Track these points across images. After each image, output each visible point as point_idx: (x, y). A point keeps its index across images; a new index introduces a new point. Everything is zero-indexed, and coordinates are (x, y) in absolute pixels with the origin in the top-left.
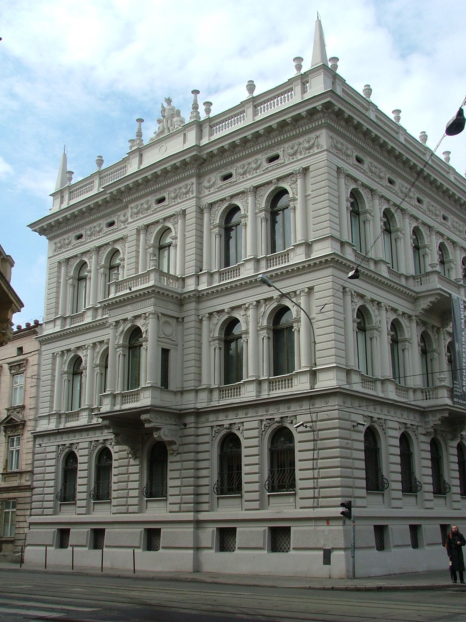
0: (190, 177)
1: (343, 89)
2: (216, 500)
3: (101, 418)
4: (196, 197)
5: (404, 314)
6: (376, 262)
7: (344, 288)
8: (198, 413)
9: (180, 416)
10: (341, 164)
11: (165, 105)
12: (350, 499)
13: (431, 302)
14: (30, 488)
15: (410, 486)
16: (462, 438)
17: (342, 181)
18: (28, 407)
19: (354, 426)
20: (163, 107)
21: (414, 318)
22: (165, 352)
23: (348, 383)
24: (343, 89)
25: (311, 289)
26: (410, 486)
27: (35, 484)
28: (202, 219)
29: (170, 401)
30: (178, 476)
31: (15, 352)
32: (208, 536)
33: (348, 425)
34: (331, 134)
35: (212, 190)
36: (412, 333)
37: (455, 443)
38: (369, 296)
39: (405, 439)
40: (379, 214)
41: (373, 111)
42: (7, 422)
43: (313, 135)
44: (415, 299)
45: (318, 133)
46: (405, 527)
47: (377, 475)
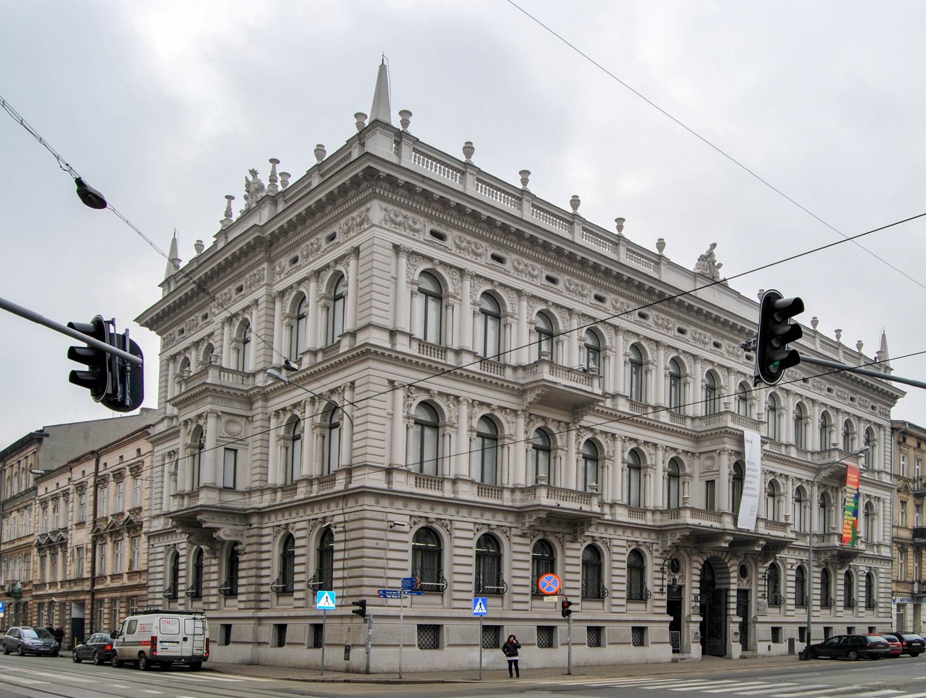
0: (260, 262)
3: (171, 518)
4: (267, 284)
5: (807, 481)
7: (391, 382)
8: (261, 513)
9: (244, 516)
10: (399, 240)
11: (251, 178)
13: (537, 395)
14: (144, 587)
15: (850, 604)
16: (775, 559)
17: (403, 261)
18: (144, 508)
19: (391, 527)
20: (247, 180)
21: (519, 413)
23: (389, 483)
25: (353, 383)
26: (850, 604)
27: (151, 583)
28: (167, 370)
30: (389, 581)
31: (135, 454)
32: (267, 632)
33: (384, 525)
34: (384, 205)
35: (282, 276)
36: (814, 494)
37: (843, 571)
39: (801, 570)
40: (863, 432)
41: (473, 175)
43: (363, 208)
44: (520, 392)
45: (368, 205)
47: (642, 586)
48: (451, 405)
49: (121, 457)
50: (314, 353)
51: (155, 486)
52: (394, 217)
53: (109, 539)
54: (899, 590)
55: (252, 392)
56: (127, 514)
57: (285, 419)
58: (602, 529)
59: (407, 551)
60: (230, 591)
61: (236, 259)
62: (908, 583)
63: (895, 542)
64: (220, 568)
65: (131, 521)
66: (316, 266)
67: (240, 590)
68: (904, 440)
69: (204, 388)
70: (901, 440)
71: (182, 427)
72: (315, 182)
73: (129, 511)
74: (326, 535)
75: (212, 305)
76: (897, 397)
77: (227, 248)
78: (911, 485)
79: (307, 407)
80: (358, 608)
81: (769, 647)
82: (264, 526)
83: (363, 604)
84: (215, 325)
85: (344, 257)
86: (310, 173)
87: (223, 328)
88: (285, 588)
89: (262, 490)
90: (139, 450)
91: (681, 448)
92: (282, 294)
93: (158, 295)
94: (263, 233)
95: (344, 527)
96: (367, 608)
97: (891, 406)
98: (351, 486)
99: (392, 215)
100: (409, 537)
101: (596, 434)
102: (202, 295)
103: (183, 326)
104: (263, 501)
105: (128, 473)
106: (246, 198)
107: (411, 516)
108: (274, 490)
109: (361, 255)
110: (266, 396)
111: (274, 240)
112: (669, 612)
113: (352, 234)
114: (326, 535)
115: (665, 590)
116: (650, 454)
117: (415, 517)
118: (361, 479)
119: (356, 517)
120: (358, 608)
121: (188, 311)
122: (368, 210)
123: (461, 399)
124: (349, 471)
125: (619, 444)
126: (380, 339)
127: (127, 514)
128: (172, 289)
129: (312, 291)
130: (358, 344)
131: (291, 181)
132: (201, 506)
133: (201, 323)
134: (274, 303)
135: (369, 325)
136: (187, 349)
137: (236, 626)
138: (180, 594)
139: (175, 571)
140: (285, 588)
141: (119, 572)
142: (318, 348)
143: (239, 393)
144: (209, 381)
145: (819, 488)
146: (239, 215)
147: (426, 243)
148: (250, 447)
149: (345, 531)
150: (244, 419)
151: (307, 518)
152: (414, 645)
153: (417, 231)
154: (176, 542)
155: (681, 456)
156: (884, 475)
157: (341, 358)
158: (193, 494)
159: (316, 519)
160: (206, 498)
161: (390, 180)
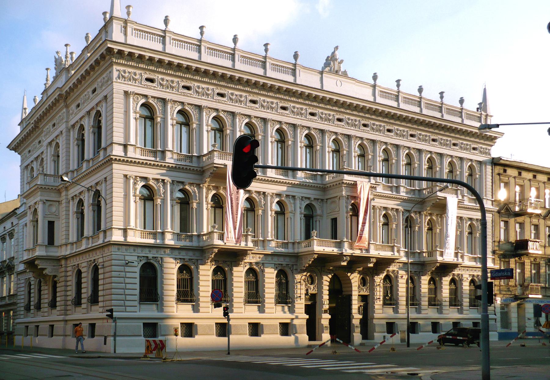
2: (90, 307)
4: (66, 122)
7: (126, 176)
8: (66, 258)
9: (58, 260)
18: (15, 257)
19: (127, 264)
22: (51, 224)
25: (106, 178)
27: (19, 301)
28: (24, 175)
29: (54, 252)
31: (10, 225)
43: (108, 72)
46: (47, 325)
49: (5, 227)
51: (20, 244)
53: (7, 273)
55: (60, 187)
56: (8, 261)
57: (76, 201)
59: (136, 278)
60: (53, 305)
61: (51, 107)
64: (49, 292)
67: (58, 304)
69: (36, 187)
70: (502, 171)
71: (28, 210)
74: (96, 269)
76: (496, 138)
77: (49, 99)
80: (109, 313)
81: (384, 337)
83: (111, 311)
85: (100, 102)
86: (83, 51)
87: (47, 149)
88: (78, 302)
89: (66, 245)
90: (12, 223)
92: (73, 126)
94: (62, 91)
95: (103, 265)
96: (114, 313)
98: (106, 241)
100: (138, 270)
103: (30, 148)
104: (66, 251)
105: (8, 238)
106: (55, 69)
107: (138, 257)
108: (72, 244)
110: (67, 187)
112: (306, 312)
113: (104, 88)
114: (96, 269)
117: (141, 257)
119: (108, 259)
120: (109, 313)
121: (58, 109)
123: (296, 197)
128: (24, 126)
131: (75, 57)
133: (52, 130)
137: (56, 325)
138: (83, 301)
139: (30, 293)
140: (78, 302)
143: (54, 188)
144: (39, 183)
146: (52, 80)
148: (60, 219)
149: (104, 268)
150: (57, 203)
152: (141, 336)
155: (313, 203)
157: (83, 174)
158: (33, 250)
160: (40, 252)
161: (120, 53)
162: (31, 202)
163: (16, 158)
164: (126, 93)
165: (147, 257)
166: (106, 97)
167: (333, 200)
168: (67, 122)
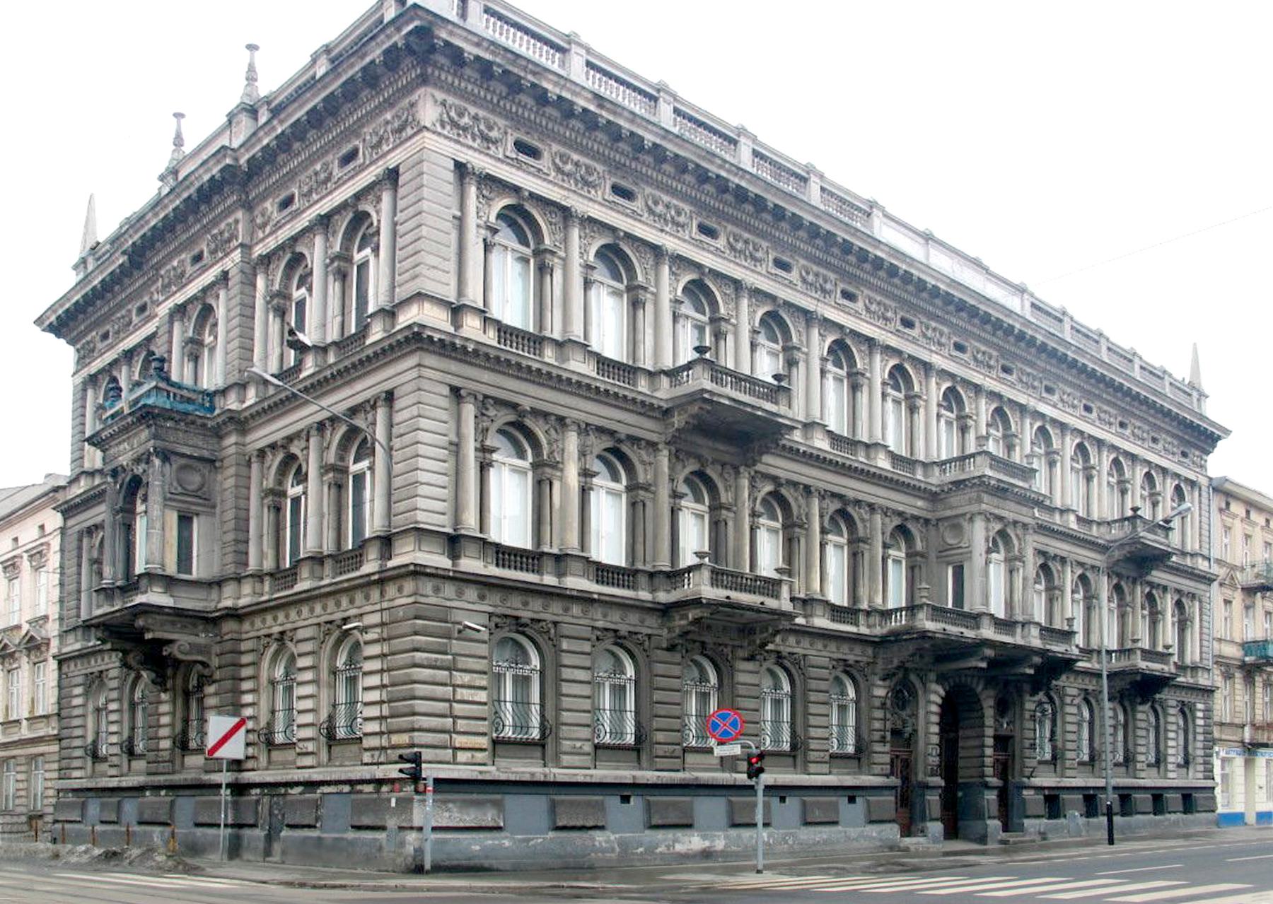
0: (229, 211)
1: (754, 150)
4: (241, 245)
5: (1093, 567)
6: (1063, 512)
7: (455, 391)
8: (235, 615)
10: (466, 156)
12: (416, 750)
13: (693, 416)
19: (460, 632)
21: (660, 446)
24: (754, 150)
28: (84, 407)
31: (35, 533)
34: (440, 96)
35: (268, 230)
38: (526, 404)
42: (28, 642)
43: (405, 102)
44: (1103, 549)
45: (414, 97)
48: (553, 432)
49: (16, 540)
50: (323, 350)
52: (456, 118)
53: (25, 659)
54: (1224, 737)
58: (792, 640)
62: (1237, 726)
63: (1217, 663)
65: (32, 638)
66: (324, 207)
68: (1228, 504)
70: (1224, 506)
72: (321, 71)
73: (30, 622)
75: (153, 289)
76: (1219, 438)
78: (1238, 574)
79: (312, 440)
82: (245, 636)
83: (417, 760)
84: (156, 320)
89: (239, 579)
90: (42, 527)
91: (623, 430)
92: (267, 260)
93: (72, 279)
97: (1208, 453)
99: (453, 114)
101: (781, 485)
102: (136, 273)
104: (245, 596)
105: (25, 564)
109: (401, 180)
111: (255, 168)
113: (385, 148)
115: (888, 735)
116: (863, 520)
118: (406, 554)
122: (412, 105)
124: (386, 542)
125: (816, 503)
126: (434, 318)
127: (26, 627)
129: (317, 253)
130: (398, 327)
132: (140, 604)
134: (255, 275)
135: (419, 296)
136: (114, 363)
141: (15, 717)
142: (329, 340)
145: (676, 457)
147: (506, 160)
148: (218, 510)
151: (315, 621)
153: (495, 142)
154: (103, 668)
156: (1200, 560)
159: (331, 622)
162: (125, 454)
163: (62, 353)
164: (461, 169)
165: (517, 618)
166: (393, 176)
167: (955, 521)
168: (246, 248)
